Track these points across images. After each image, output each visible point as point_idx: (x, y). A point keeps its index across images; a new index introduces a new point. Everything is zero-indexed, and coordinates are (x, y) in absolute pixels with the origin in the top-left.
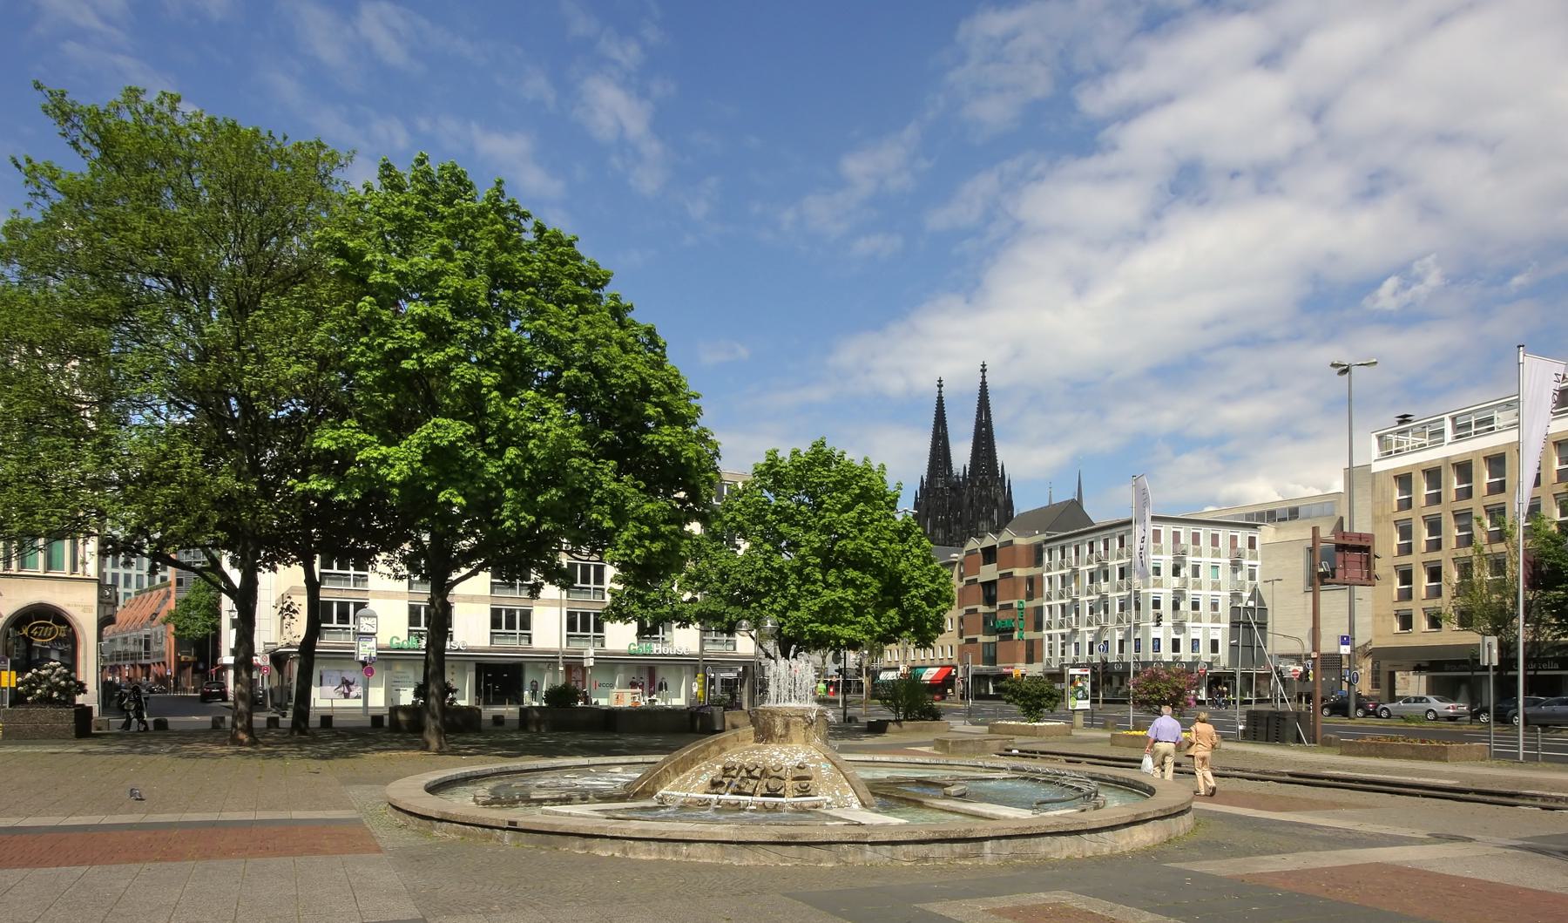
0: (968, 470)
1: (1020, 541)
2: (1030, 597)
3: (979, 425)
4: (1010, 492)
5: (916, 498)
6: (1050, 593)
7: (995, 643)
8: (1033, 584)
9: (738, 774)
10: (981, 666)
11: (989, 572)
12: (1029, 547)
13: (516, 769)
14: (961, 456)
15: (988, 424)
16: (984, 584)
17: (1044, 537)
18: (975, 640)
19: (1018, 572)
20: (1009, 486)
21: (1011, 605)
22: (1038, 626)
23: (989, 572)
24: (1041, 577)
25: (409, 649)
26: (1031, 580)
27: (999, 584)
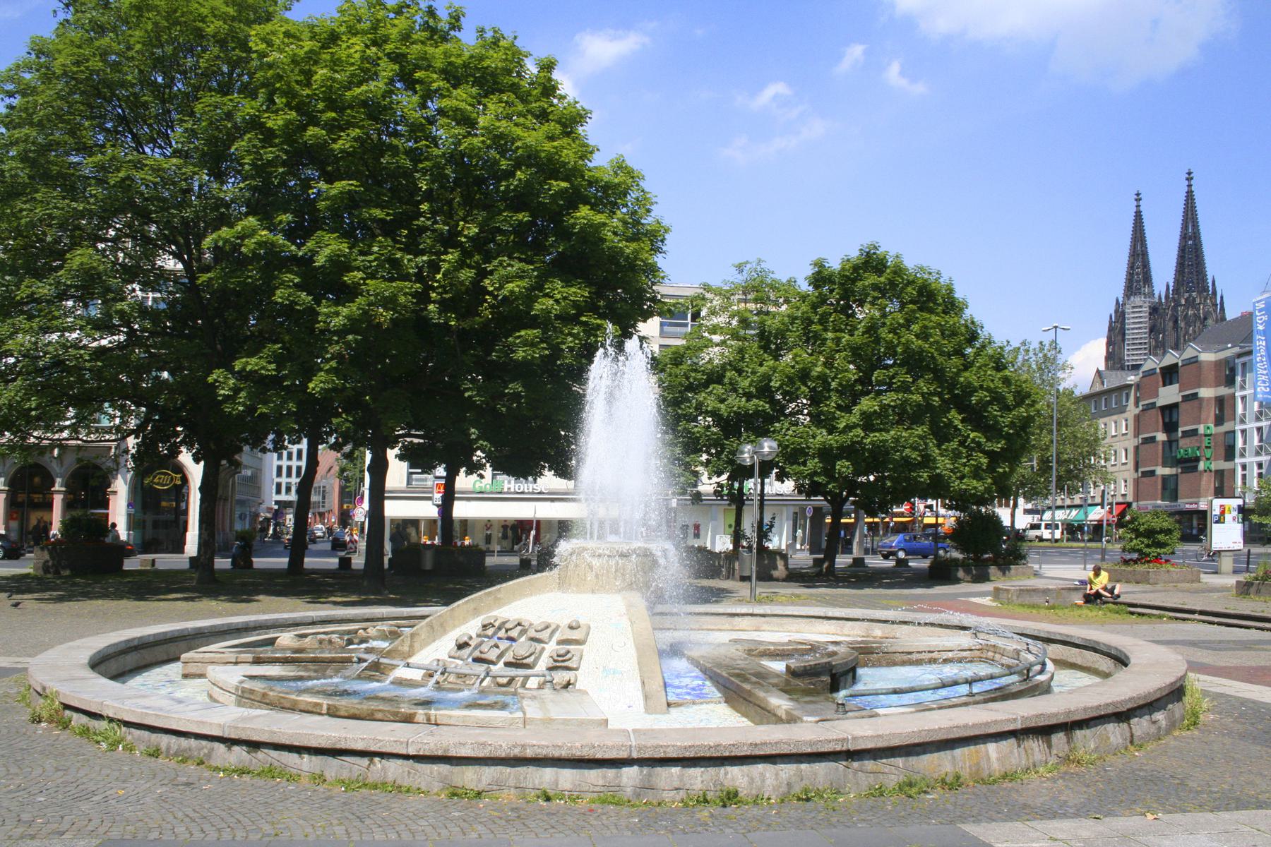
0: (1171, 288)
1: (1207, 357)
2: (1219, 421)
3: (1184, 237)
4: (1222, 309)
5: (1111, 323)
6: (1244, 415)
7: (1177, 475)
8: (1224, 408)
9: (495, 633)
10: (1159, 502)
11: (1169, 394)
12: (1218, 364)
13: (348, 617)
14: (1163, 273)
15: (1196, 237)
16: (1163, 408)
17: (1237, 350)
18: (1152, 473)
19: (1206, 393)
20: (1222, 297)
21: (1195, 432)
22: (1230, 453)
23: (1169, 394)
24: (1233, 397)
25: (492, 493)
26: (1220, 401)
27: (1182, 407)
